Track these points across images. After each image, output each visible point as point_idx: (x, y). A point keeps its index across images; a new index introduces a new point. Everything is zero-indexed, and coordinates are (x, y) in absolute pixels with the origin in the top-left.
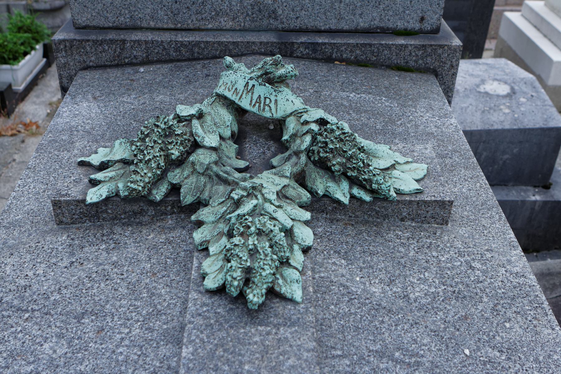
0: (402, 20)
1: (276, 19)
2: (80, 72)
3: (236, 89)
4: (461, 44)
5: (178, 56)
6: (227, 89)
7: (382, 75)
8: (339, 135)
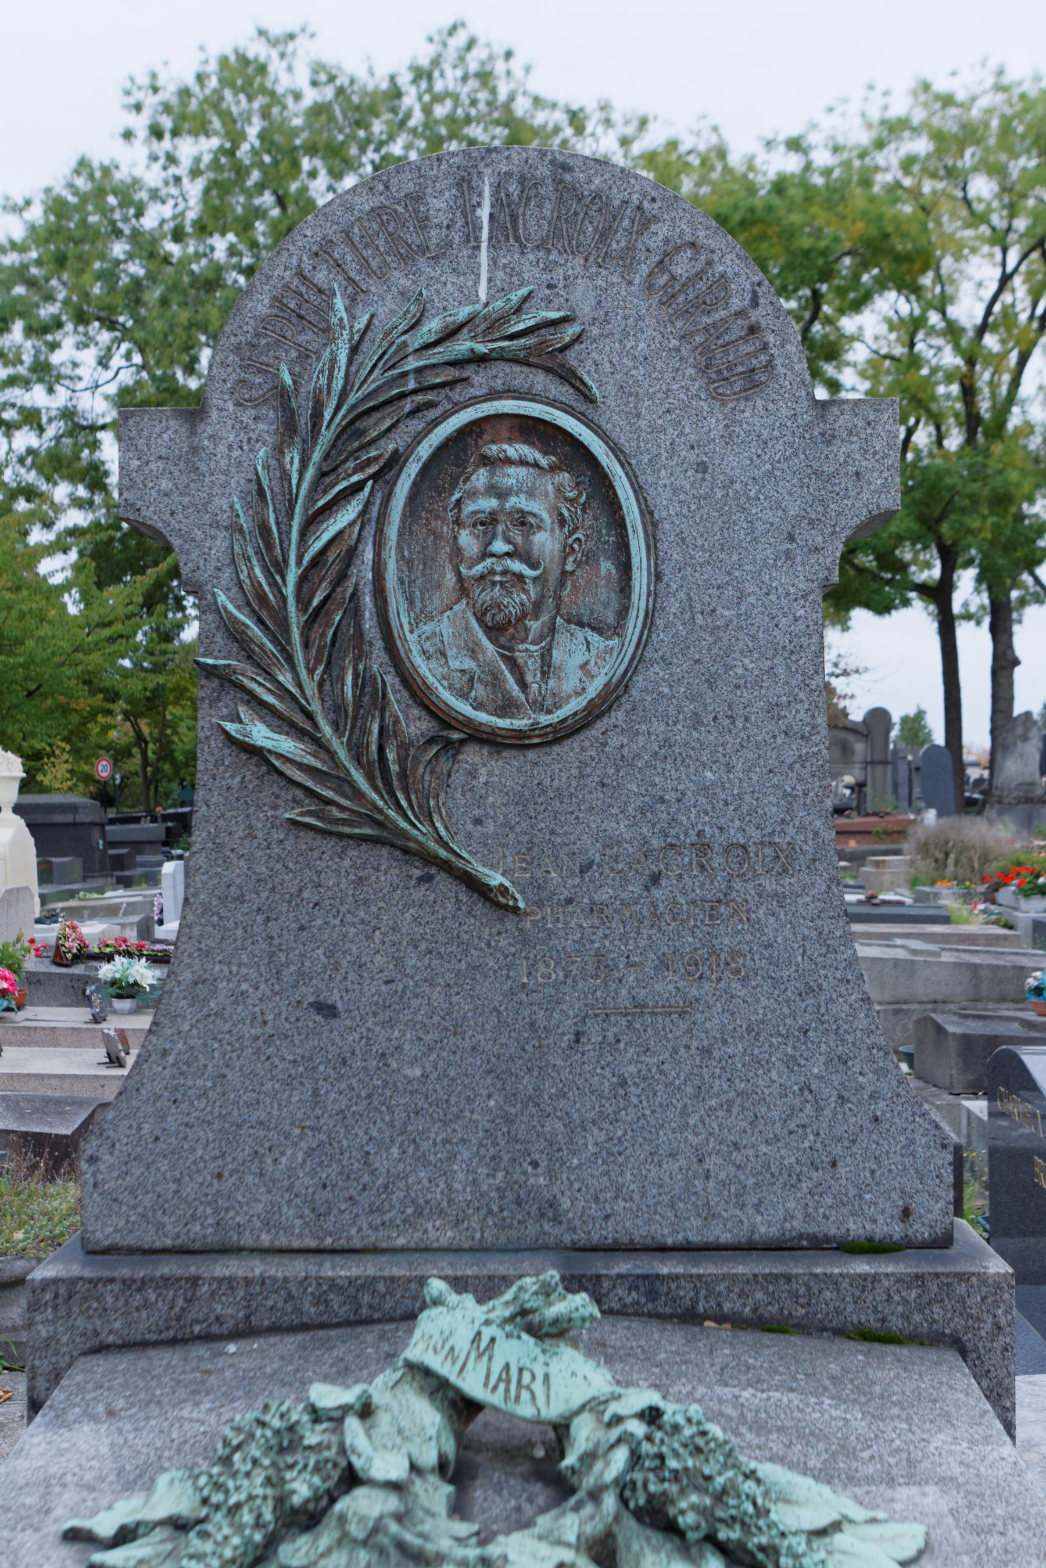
0: (858, 1216)
1: (556, 1220)
2: (83, 1359)
3: (452, 1349)
4: (1011, 1270)
5: (321, 1314)
6: (431, 1350)
7: (824, 1351)
8: (692, 1437)
